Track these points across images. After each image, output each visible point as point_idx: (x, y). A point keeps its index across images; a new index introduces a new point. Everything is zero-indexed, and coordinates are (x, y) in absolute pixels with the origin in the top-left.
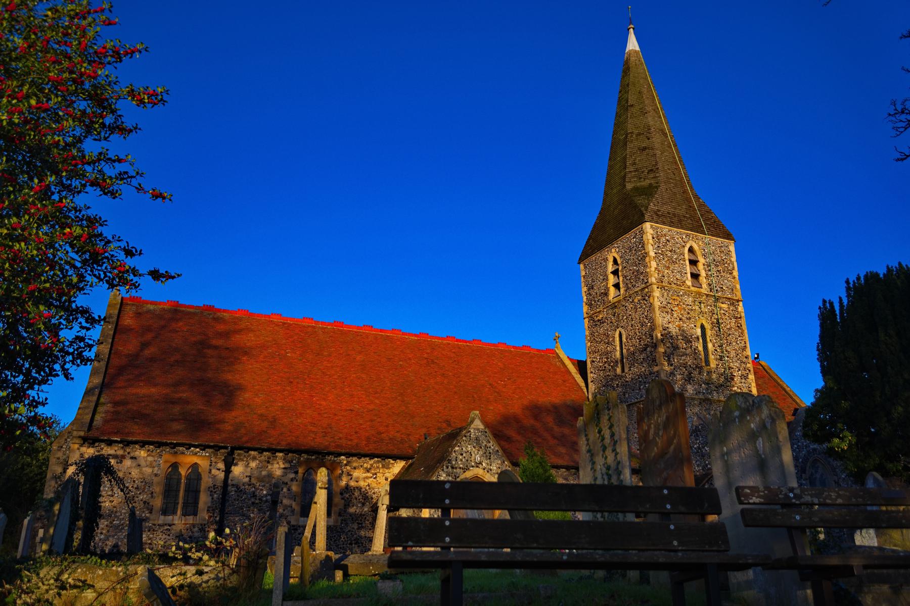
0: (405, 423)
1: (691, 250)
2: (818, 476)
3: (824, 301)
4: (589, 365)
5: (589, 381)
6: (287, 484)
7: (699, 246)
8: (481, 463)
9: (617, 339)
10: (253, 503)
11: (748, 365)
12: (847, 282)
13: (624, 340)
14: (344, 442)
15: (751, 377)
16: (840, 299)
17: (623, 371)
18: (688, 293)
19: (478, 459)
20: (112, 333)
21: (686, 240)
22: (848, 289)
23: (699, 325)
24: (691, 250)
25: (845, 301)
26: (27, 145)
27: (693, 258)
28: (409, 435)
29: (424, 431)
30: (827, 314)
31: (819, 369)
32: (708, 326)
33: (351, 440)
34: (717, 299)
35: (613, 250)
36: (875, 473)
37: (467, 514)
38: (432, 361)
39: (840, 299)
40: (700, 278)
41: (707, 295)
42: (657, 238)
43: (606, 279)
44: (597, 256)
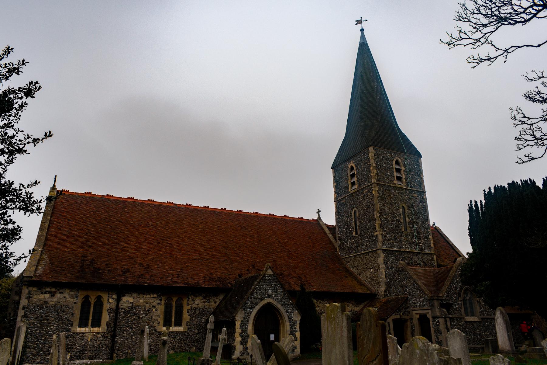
0: (228, 267)
1: (397, 163)
2: (468, 298)
3: (471, 201)
4: (337, 230)
5: (337, 239)
6: (155, 307)
7: (401, 160)
8: (271, 295)
9: (353, 215)
10: (134, 319)
11: (429, 230)
12: (484, 191)
13: (358, 215)
14: (190, 281)
15: (431, 237)
16: (481, 201)
17: (356, 234)
18: (395, 188)
20: (50, 213)
22: (485, 194)
23: (401, 206)
25: (483, 202)
27: (398, 167)
28: (229, 275)
29: (238, 272)
30: (473, 211)
31: (469, 241)
32: (406, 208)
33: (194, 279)
34: (412, 191)
35: (351, 162)
36: (500, 308)
38: (245, 227)
39: (481, 201)
41: (406, 189)
42: (376, 155)
44: (343, 166)
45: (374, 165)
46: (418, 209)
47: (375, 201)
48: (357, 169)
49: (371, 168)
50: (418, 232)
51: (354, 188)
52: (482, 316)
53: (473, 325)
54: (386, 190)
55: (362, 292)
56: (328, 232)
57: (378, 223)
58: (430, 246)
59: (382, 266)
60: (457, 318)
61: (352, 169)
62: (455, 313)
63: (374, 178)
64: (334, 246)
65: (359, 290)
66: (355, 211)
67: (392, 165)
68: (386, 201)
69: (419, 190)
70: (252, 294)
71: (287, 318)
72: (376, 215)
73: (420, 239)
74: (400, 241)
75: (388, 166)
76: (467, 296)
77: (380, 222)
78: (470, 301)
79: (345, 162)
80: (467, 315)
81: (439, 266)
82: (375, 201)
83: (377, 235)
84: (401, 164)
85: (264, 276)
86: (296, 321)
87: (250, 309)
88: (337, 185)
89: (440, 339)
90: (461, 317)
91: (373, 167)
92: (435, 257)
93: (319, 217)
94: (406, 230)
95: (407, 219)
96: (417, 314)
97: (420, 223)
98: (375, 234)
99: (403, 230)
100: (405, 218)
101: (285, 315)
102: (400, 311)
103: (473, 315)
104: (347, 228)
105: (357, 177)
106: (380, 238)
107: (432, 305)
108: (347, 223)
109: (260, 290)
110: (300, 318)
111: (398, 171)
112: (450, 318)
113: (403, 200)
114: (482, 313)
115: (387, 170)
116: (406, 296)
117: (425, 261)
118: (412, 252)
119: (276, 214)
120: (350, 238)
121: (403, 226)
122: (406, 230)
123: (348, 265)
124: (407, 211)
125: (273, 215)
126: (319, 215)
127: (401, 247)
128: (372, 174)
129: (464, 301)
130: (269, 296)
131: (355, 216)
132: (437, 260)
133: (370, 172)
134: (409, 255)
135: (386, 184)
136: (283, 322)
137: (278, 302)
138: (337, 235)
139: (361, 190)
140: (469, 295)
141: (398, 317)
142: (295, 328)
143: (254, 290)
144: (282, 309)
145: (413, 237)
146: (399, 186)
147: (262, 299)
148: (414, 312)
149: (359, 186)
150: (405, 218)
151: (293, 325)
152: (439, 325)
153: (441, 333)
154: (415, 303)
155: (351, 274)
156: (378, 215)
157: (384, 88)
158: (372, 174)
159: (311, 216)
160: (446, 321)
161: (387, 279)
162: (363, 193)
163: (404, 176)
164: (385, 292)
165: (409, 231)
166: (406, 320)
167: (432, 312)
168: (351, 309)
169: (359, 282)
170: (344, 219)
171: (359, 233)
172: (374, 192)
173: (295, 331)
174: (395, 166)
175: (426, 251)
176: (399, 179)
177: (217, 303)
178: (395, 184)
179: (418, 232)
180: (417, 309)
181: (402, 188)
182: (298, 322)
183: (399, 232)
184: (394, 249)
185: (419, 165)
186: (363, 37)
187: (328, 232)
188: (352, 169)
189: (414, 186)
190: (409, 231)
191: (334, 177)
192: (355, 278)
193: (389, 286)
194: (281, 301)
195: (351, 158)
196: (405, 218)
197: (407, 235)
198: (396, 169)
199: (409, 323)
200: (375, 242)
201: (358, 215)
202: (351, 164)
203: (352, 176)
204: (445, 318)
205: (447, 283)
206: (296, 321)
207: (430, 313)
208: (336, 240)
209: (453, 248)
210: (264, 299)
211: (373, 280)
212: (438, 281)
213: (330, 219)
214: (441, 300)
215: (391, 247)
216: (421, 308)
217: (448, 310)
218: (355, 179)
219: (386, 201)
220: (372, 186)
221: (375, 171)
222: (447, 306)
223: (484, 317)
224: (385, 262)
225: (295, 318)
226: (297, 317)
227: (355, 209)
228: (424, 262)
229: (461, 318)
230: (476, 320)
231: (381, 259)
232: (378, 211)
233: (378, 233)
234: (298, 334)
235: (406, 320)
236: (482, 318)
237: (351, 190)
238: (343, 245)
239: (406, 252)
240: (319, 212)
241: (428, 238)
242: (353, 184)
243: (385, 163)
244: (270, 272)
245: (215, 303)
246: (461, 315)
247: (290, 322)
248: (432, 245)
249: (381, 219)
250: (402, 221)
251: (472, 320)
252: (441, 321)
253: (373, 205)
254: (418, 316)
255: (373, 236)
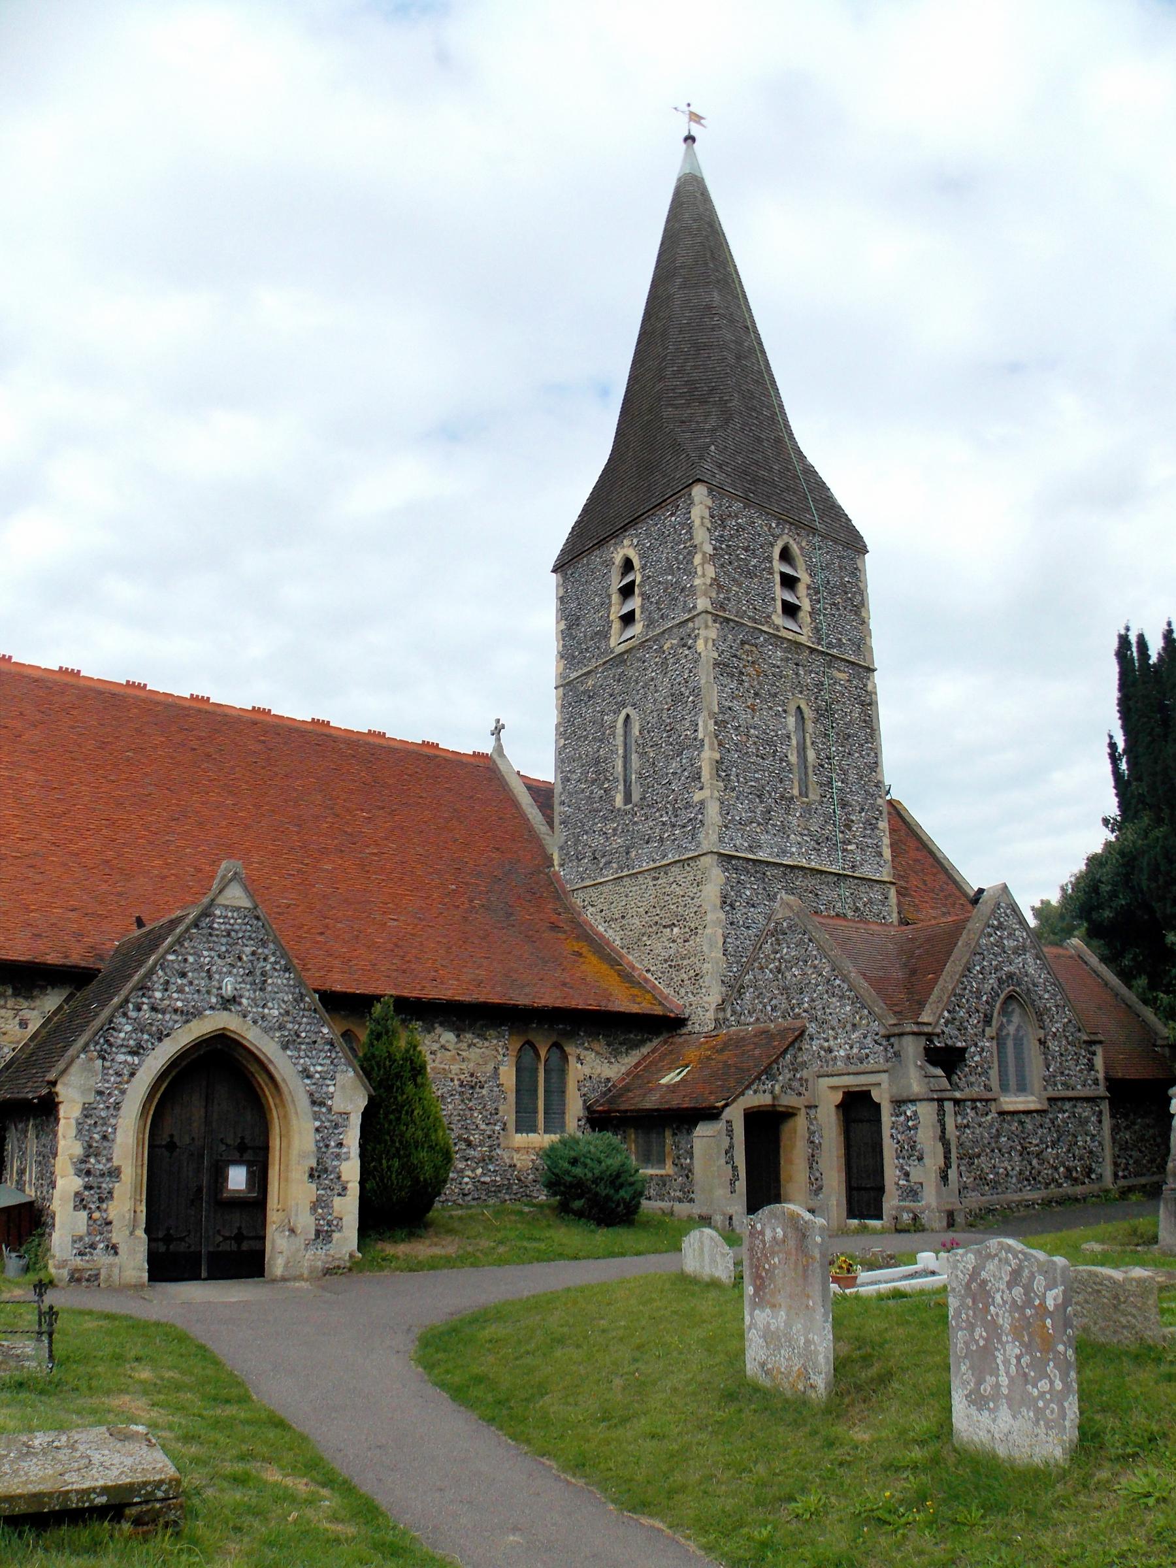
2: (1011, 1029)
5: (557, 821)
7: (802, 548)
8: (234, 1000)
9: (620, 730)
11: (880, 801)
13: (636, 731)
15: (883, 825)
17: (628, 799)
19: (228, 989)
21: (777, 531)
23: (792, 708)
24: (786, 555)
26: (979, 1383)
32: (808, 713)
35: (626, 542)
37: (303, 1156)
40: (801, 614)
43: (606, 605)
44: (596, 558)
45: (709, 549)
46: (848, 725)
47: (705, 676)
48: (643, 568)
49: (697, 559)
50: (844, 805)
51: (629, 633)
52: (1051, 1093)
53: (1021, 1123)
54: (743, 643)
55: (635, 1009)
56: (525, 799)
57: (708, 756)
58: (880, 855)
59: (715, 917)
60: (974, 1101)
61: (628, 566)
62: (972, 1084)
63: (705, 594)
64: (542, 847)
65: (623, 1002)
66: (628, 716)
67: (769, 559)
68: (741, 682)
69: (852, 658)
70: (143, 988)
71: (303, 1102)
72: (705, 727)
73: (849, 828)
74: (784, 830)
75: (754, 562)
76: (1009, 1022)
77: (717, 756)
78: (1019, 1042)
79: (602, 543)
80: (1004, 1088)
81: (904, 922)
82: (705, 676)
83: (702, 802)
84: (800, 561)
85: (206, 913)
86: (346, 1115)
87: (133, 1053)
88: (569, 628)
89: (913, 1178)
90: (989, 1095)
91: (704, 554)
92: (893, 892)
93: (499, 748)
94: (804, 793)
95: (811, 754)
96: (832, 1088)
97: (852, 777)
98: (697, 796)
99: (796, 792)
100: (802, 750)
101: (295, 1088)
102: (772, 1078)
103: (1022, 1088)
104: (594, 782)
105: (642, 594)
106: (713, 811)
107: (897, 1054)
108: (597, 763)
109: (183, 975)
110: (362, 1103)
111: (789, 582)
112: (957, 1102)
113: (800, 687)
114: (1049, 1080)
115: (750, 575)
116: (798, 1023)
117: (860, 905)
118: (822, 872)
119: (339, 721)
120: (605, 818)
121: (794, 777)
122: (804, 793)
123: (590, 916)
124: (810, 726)
125: (327, 724)
126: (498, 739)
127: (784, 852)
128: (697, 582)
129: (1000, 1040)
130: (228, 1003)
131: (626, 734)
132: (899, 904)
133: (692, 574)
134: (811, 882)
135: (745, 621)
136: (285, 1117)
137: (266, 1030)
138: (558, 809)
139: (655, 639)
140: (1016, 1019)
141: (766, 1099)
142: (340, 1145)
143: (152, 972)
144: (283, 1064)
145: (829, 818)
146: (790, 636)
147: (189, 1015)
148: (825, 1082)
149: (650, 624)
150: (804, 749)
151: (329, 1131)
152: (915, 1128)
153: (920, 1159)
154: (830, 1050)
155: (600, 948)
156: (712, 727)
157: (751, 316)
158: (697, 582)
159: (464, 737)
160: (941, 1112)
161: (730, 965)
162: (661, 650)
163: (806, 605)
164: (721, 1008)
165: (814, 796)
166: (789, 1114)
167: (891, 1082)
168: (587, 1071)
169: (627, 977)
170: (587, 749)
171: (636, 797)
172: (700, 645)
173: (338, 1156)
174: (779, 567)
175: (866, 871)
176: (791, 610)
177: (33, 1027)
178: (777, 628)
179: (844, 805)
180: (835, 1070)
181: (798, 645)
182: (356, 1121)
183: (782, 797)
184: (762, 855)
185: (856, 573)
186: (690, 156)
187: (525, 799)
188: (628, 566)
189: (840, 644)
190: (814, 796)
191: (561, 599)
192: (611, 959)
193: (734, 989)
194: (281, 1027)
195: (624, 528)
196: (802, 750)
197: (808, 810)
198: (783, 574)
199: (800, 1123)
200: (695, 826)
201: (636, 731)
202: (626, 549)
203: (627, 591)
204: (940, 1101)
205: (953, 968)
206: (346, 1115)
207: (885, 1086)
208: (552, 826)
209: (945, 871)
210: (197, 1014)
211: (678, 968)
212: (917, 966)
213: (534, 757)
214: (929, 1036)
215: (750, 849)
216: (853, 1069)
217: (949, 1073)
218: (635, 603)
219: (741, 682)
220: (698, 622)
221: (711, 571)
222: (947, 1058)
223: (1056, 1094)
224: (727, 903)
225: (338, 1104)
226: (350, 1098)
227: (629, 710)
228: (857, 909)
229: (987, 1101)
230: (1032, 1107)
231: (711, 891)
232: (712, 715)
233: (708, 794)
234: (351, 1170)
235: (789, 1114)
236: (1049, 1099)
237: (618, 639)
238: (577, 842)
239: (802, 868)
240: (498, 730)
241: (874, 828)
242: (628, 619)
243: (746, 549)
244: (236, 896)
245: (23, 1024)
246: (988, 1088)
247: (316, 1116)
248: (887, 853)
249: (720, 744)
250: (793, 758)
251: (1021, 1107)
252: (926, 1112)
253: (696, 692)
254: (838, 1097)
255: (688, 806)
